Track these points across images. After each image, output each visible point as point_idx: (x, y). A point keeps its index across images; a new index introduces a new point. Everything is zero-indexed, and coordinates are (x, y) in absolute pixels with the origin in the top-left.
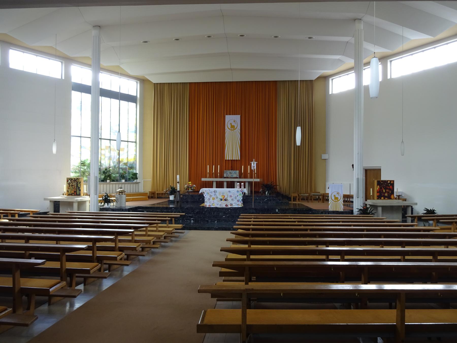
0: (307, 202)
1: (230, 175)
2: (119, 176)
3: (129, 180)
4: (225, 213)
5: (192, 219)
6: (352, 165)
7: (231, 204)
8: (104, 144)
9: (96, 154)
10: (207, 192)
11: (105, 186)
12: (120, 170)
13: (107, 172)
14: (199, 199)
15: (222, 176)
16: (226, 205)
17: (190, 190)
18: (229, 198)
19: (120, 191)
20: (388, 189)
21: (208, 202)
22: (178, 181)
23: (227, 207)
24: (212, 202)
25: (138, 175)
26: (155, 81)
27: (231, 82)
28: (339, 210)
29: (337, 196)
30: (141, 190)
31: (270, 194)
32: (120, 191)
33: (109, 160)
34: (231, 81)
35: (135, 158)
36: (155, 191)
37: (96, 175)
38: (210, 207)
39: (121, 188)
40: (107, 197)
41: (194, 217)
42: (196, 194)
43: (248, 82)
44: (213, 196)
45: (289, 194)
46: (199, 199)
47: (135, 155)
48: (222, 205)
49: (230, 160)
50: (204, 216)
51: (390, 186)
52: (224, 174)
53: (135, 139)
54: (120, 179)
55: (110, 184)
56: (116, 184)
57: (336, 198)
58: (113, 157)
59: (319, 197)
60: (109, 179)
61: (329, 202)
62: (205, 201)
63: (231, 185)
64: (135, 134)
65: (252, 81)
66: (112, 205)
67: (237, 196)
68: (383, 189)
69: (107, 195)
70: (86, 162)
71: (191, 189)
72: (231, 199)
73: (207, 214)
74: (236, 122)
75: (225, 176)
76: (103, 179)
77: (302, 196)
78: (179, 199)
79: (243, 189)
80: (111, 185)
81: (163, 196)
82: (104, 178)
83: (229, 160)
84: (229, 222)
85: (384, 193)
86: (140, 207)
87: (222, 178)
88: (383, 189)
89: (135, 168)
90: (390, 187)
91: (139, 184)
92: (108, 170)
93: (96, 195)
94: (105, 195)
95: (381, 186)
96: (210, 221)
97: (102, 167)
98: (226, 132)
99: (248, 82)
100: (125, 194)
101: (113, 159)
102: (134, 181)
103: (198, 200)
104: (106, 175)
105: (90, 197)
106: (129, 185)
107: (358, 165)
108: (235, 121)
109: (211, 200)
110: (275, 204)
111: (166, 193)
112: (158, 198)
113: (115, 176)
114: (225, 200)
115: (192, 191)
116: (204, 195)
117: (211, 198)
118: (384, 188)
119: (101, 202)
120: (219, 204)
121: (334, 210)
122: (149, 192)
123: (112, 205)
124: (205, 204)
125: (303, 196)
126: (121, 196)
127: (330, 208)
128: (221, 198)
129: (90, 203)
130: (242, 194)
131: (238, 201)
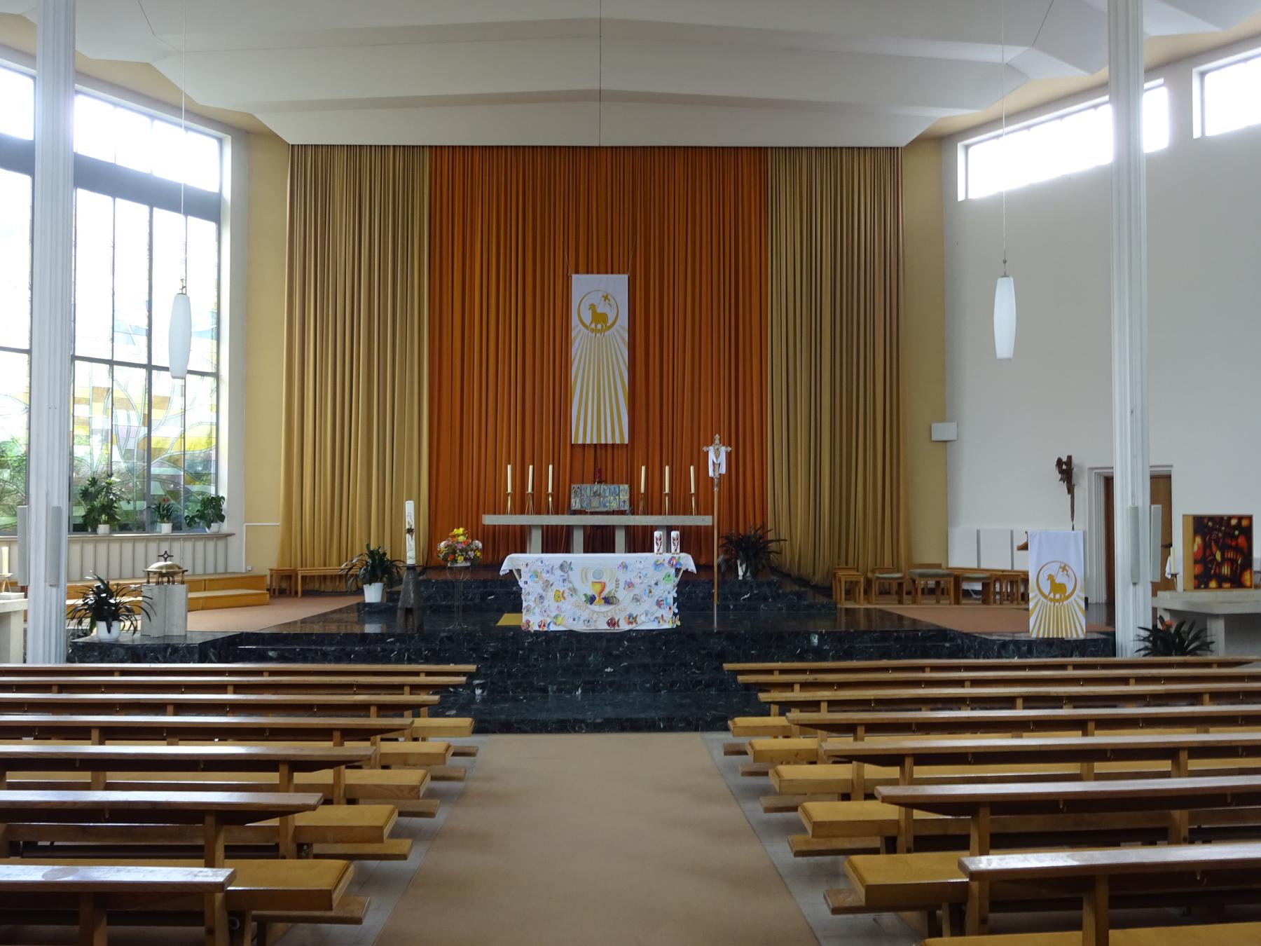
0: (934, 602)
1: (595, 504)
2: (149, 507)
3: (191, 522)
4: (610, 654)
5: (477, 682)
6: (1056, 459)
7: (630, 616)
8: (87, 377)
9: (58, 411)
10: (532, 570)
11: (89, 548)
12: (153, 483)
13: (99, 492)
14: (483, 597)
15: (562, 507)
16: (612, 623)
17: (461, 562)
18: (622, 594)
19: (164, 571)
20: (1230, 547)
21: (537, 610)
22: (407, 527)
23: (616, 629)
24: (551, 608)
25: (225, 506)
26: (291, 143)
27: (593, 147)
28: (1064, 636)
29: (1060, 579)
30: (238, 563)
31: (754, 575)
32: (161, 568)
33: (104, 447)
34: (596, 144)
35: (214, 435)
36: (296, 566)
37: (55, 503)
38: (546, 629)
39: (166, 556)
40: (104, 595)
41: (485, 675)
42: (488, 575)
43: (657, 150)
44: (559, 586)
45: (814, 573)
46: (483, 597)
47: (214, 427)
48: (595, 620)
49: (589, 445)
50: (527, 669)
51: (1238, 535)
52: (573, 500)
53: (215, 362)
54: (153, 523)
55: (109, 540)
56: (134, 540)
57: (1057, 588)
58: (122, 432)
59: (938, 583)
60: (105, 523)
61: (1031, 604)
62: (524, 604)
63: (640, 541)
64: (215, 342)
65: (674, 148)
66: (126, 628)
67: (656, 584)
68: (1214, 547)
69: (107, 586)
70: (11, 450)
71: (466, 559)
72: (632, 594)
73: (536, 660)
74: (612, 302)
75: (576, 504)
76: (80, 521)
77: (878, 578)
78: (414, 597)
79: (675, 555)
80: (115, 547)
81: (329, 587)
82: (83, 517)
83: (584, 445)
84: (634, 693)
85: (1220, 565)
86: (247, 633)
87: (563, 513)
88: (1214, 547)
89: (213, 477)
90: (1240, 540)
91: (229, 538)
92: (103, 484)
93: (54, 590)
94: (98, 587)
95: (1207, 538)
96: (555, 687)
97: (77, 473)
98: (575, 340)
99: (657, 150)
100: (183, 582)
101: (122, 443)
102: (209, 527)
103: (477, 601)
104: (93, 506)
105: (26, 597)
106: (189, 545)
107: (1134, 457)
108: (609, 297)
109: (550, 601)
110: (784, 611)
111: (352, 575)
112: (309, 593)
113: (130, 507)
114: (607, 601)
115: (468, 564)
116: (521, 583)
117: (550, 595)
118: (1217, 544)
119: (73, 613)
120: (583, 618)
121: (1051, 636)
122: (271, 570)
123: (123, 631)
124: (525, 617)
125: (882, 581)
126: (166, 590)
127: (1033, 630)
128: (590, 593)
129: (25, 621)
130: (677, 576)
131: (659, 604)
